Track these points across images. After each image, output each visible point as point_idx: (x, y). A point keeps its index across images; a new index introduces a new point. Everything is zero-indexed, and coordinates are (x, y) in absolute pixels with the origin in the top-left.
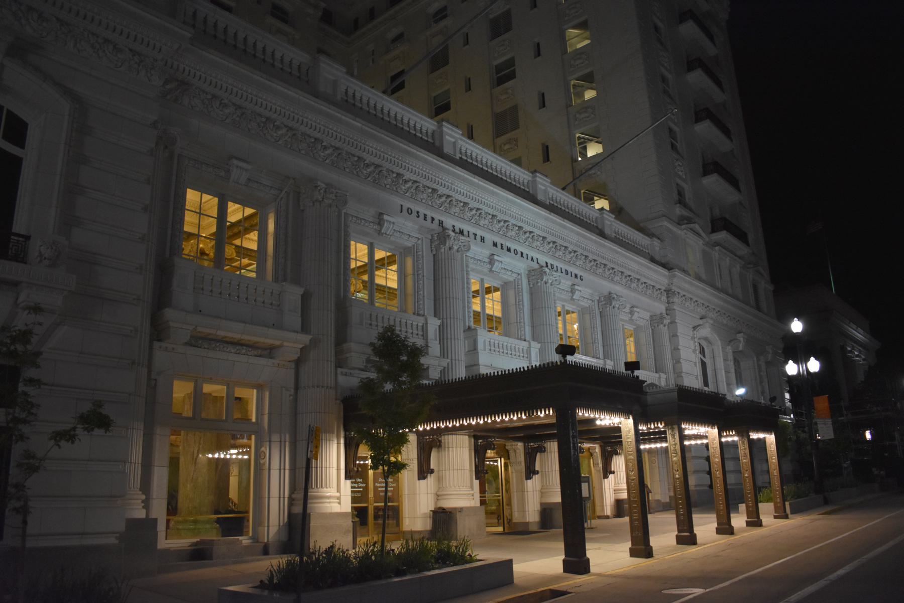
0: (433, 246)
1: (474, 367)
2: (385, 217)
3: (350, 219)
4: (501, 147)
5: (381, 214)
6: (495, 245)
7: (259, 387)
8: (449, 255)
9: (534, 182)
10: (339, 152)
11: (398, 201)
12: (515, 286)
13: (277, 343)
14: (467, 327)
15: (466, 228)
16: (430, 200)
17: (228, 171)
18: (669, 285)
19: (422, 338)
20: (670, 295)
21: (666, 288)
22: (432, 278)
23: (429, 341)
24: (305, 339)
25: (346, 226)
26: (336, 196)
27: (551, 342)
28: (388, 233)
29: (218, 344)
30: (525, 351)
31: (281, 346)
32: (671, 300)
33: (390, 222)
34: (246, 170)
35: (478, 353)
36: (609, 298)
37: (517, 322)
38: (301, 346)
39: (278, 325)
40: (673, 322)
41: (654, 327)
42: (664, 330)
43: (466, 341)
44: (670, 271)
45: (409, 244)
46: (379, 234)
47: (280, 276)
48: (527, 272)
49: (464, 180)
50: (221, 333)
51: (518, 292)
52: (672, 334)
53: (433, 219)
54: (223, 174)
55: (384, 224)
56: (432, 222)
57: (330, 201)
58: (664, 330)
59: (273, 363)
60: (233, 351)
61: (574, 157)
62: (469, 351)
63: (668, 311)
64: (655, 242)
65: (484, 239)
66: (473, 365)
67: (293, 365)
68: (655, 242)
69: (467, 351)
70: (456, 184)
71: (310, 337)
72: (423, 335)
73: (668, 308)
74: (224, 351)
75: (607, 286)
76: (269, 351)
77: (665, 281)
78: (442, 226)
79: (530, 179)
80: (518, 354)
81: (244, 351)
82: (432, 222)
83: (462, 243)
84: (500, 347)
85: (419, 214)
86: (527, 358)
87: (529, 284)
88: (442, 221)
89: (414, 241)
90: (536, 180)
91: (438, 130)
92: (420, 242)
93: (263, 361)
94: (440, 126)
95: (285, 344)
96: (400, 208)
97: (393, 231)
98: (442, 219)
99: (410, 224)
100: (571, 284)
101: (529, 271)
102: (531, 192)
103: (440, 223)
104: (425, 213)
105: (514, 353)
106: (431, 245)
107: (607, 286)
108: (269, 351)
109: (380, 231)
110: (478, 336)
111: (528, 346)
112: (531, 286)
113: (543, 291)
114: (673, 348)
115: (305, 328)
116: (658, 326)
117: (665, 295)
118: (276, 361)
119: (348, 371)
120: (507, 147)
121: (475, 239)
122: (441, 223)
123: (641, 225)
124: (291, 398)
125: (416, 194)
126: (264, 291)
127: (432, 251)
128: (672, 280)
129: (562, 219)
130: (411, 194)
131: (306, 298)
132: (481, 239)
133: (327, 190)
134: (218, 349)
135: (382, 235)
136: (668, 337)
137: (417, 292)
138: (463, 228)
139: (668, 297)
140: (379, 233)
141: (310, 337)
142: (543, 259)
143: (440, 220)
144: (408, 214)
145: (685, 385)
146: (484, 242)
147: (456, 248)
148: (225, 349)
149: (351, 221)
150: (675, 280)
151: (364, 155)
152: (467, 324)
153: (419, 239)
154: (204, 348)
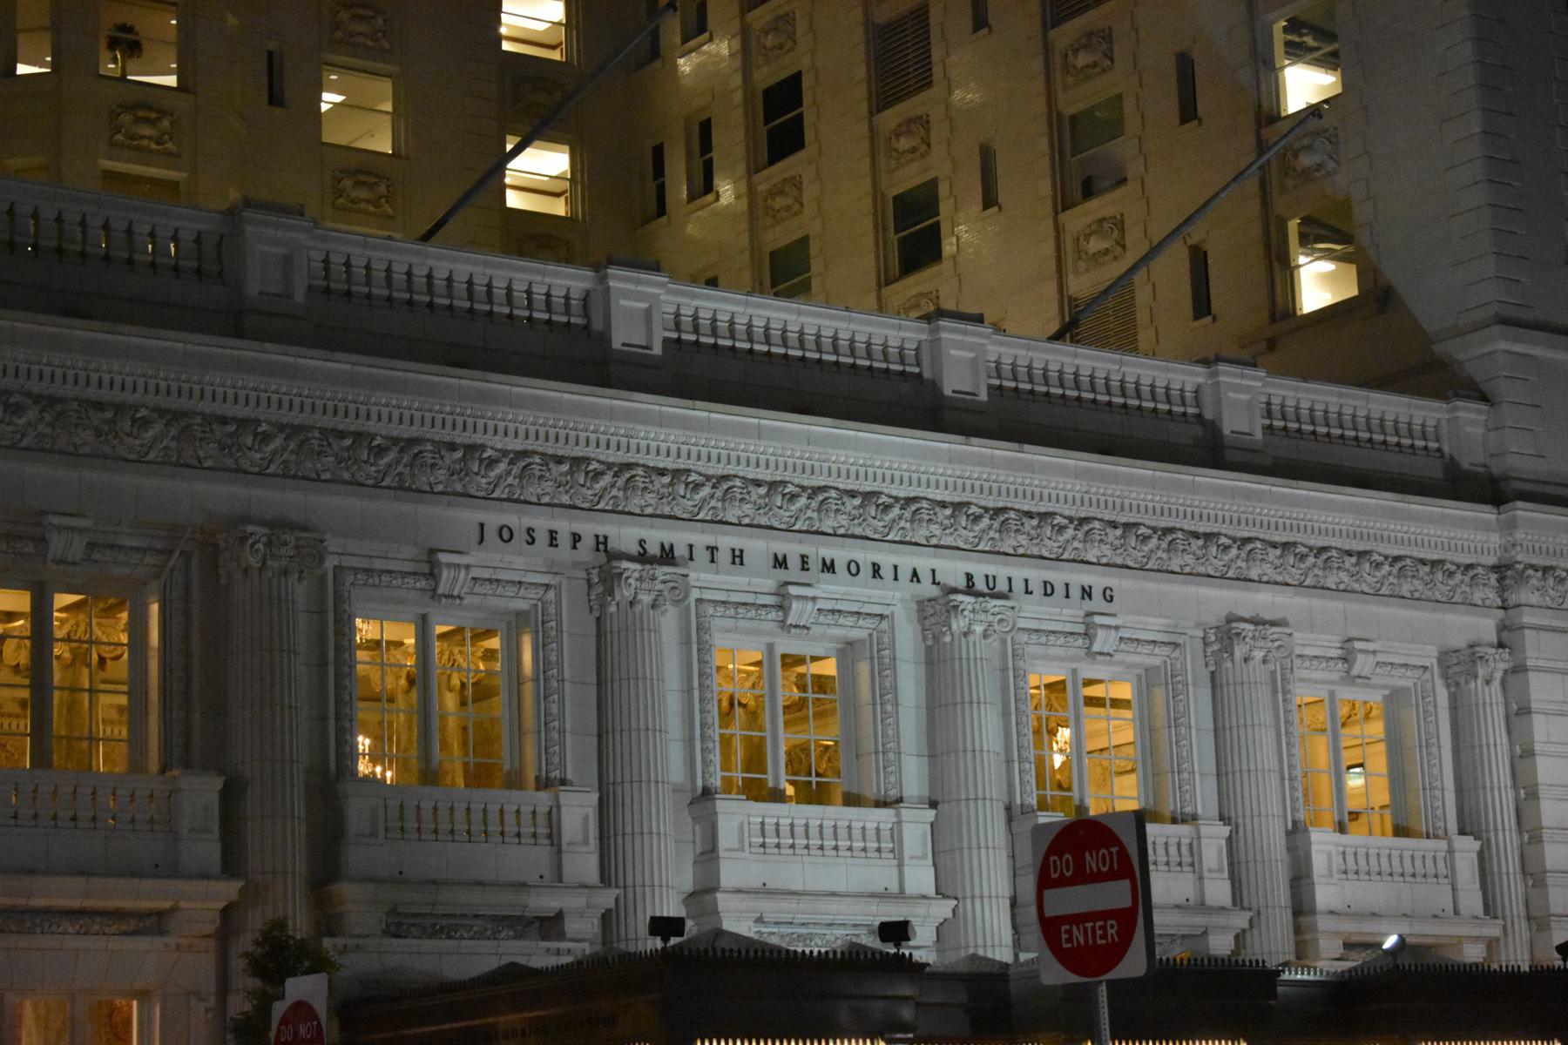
0: (593, 597)
1: (707, 897)
2: (444, 558)
3: (351, 578)
4: (1066, 55)
5: (433, 552)
6: (780, 562)
7: (144, 996)
8: (630, 617)
9: (935, 343)
10: (302, 437)
11: (468, 516)
12: (871, 652)
13: (167, 905)
14: (700, 791)
15: (679, 537)
16: (567, 492)
17: (42, 541)
18: (1506, 551)
19: (547, 842)
20: (1507, 582)
21: (1500, 559)
22: (594, 679)
23: (564, 848)
24: (229, 889)
25: (339, 599)
26: (297, 547)
27: (984, 799)
28: (455, 593)
29: (38, 921)
30: (885, 834)
31: (174, 910)
32: (1513, 599)
33: (459, 566)
34: (81, 531)
35: (718, 858)
36: (1227, 633)
37: (876, 753)
38: (221, 905)
39: (169, 869)
40: (1519, 669)
41: (1457, 684)
42: (1490, 698)
43: (697, 827)
44: (1502, 508)
45: (523, 605)
46: (433, 597)
47: (179, 755)
48: (915, 607)
49: (662, 421)
50: (40, 902)
51: (884, 667)
52: (1515, 707)
53: (576, 538)
54: (30, 548)
55: (440, 575)
56: (574, 547)
57: (284, 562)
58: (1490, 698)
59: (166, 945)
60: (71, 930)
61: (1265, 104)
62: (702, 853)
63: (1505, 634)
64: (1459, 414)
65: (741, 557)
66: (703, 894)
67: (211, 944)
68: (1459, 414)
69: (699, 850)
70: (642, 434)
71: (240, 884)
72: (550, 836)
73: (1508, 623)
74: (52, 933)
75: (1220, 599)
76: (155, 922)
77: (1495, 540)
78: (606, 550)
79: (924, 337)
80: (858, 845)
81: (96, 928)
82: (574, 547)
83: (664, 582)
84: (811, 835)
85: (534, 535)
86: (892, 851)
87: (924, 639)
88: (606, 538)
89: (533, 594)
90: (939, 339)
91: (600, 288)
92: (551, 594)
93: (143, 943)
94: (603, 280)
95: (183, 904)
96: (478, 528)
97: (469, 584)
98: (601, 530)
99: (519, 562)
100: (1082, 613)
101: (921, 611)
102: (927, 375)
103: (598, 543)
104: (553, 528)
105: (858, 845)
106: (589, 595)
107: (1220, 599)
108: (155, 922)
109: (434, 590)
110: (720, 817)
111: (895, 820)
112: (930, 643)
113: (957, 656)
114: (1518, 750)
115: (231, 865)
116: (1466, 682)
117: (1493, 582)
118: (172, 941)
119: (351, 942)
120: (1082, 59)
121: (713, 561)
122: (601, 543)
123: (1438, 349)
124: (210, 1015)
125: (522, 487)
126: (132, 795)
127: (591, 608)
128: (1511, 534)
129: (1016, 446)
130: (507, 490)
131: (231, 795)
132: (734, 556)
133: (274, 538)
134: (38, 930)
135: (440, 601)
136: (1499, 712)
137: (546, 724)
138: (673, 541)
139: (1502, 589)
140: (434, 594)
141: (240, 884)
142: (953, 569)
143: (597, 537)
144: (499, 541)
145: (1212, 952)
146: (742, 564)
147: (646, 599)
148: (54, 928)
149: (352, 584)
150: (1520, 535)
151: (372, 426)
152: (699, 783)
153: (547, 586)
154: (11, 932)
